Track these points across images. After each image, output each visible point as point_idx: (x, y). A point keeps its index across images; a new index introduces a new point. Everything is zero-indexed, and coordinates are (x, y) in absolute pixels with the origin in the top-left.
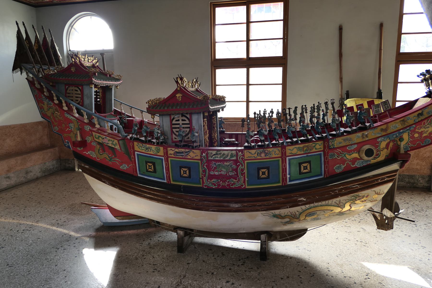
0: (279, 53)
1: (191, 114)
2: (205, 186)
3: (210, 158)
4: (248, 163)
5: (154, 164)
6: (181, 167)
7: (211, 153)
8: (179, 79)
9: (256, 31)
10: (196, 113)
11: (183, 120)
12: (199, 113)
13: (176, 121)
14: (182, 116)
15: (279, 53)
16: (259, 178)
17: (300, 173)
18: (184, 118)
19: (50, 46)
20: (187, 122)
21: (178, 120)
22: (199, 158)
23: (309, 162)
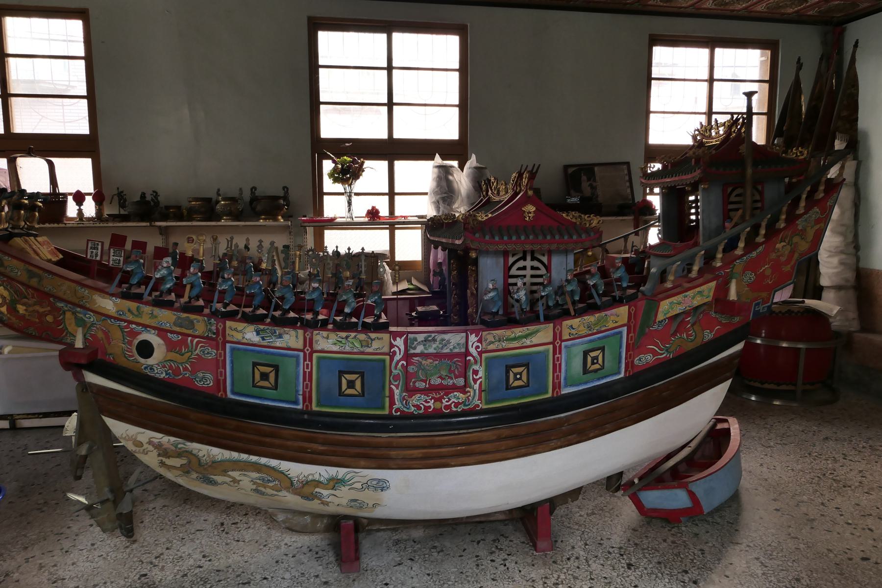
0: (82, 127)
1: (550, 253)
2: (397, 410)
3: (412, 351)
4: (319, 358)
5: (276, 368)
6: (341, 373)
7: (416, 339)
8: (526, 175)
9: (374, 87)
10: (559, 252)
11: (533, 268)
12: (566, 252)
13: (519, 269)
14: (532, 260)
15: (82, 127)
16: (508, 387)
17: (585, 371)
18: (536, 264)
19: (845, 75)
20: (543, 271)
21: (524, 268)
22: (386, 349)
23: (603, 349)
